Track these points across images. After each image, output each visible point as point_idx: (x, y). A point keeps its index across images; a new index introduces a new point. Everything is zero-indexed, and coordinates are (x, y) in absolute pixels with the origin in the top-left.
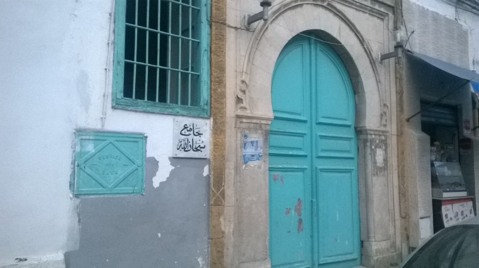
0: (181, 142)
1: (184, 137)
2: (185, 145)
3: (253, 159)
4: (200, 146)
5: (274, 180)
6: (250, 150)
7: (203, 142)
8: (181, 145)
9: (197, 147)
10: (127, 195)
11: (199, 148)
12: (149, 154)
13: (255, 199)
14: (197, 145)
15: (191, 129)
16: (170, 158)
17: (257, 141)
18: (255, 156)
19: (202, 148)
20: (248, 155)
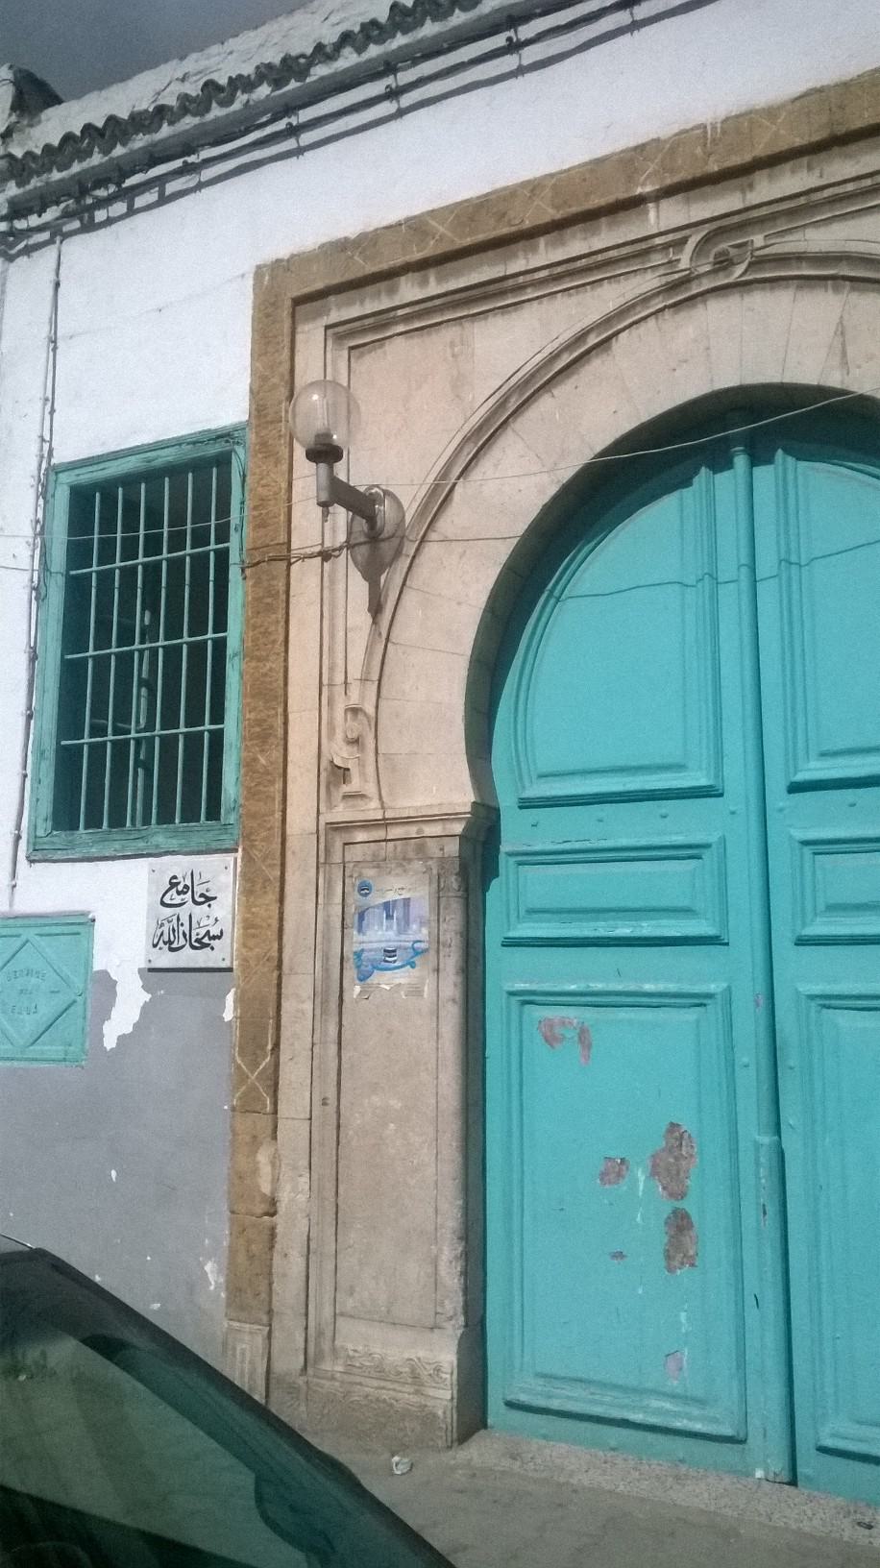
0: (162, 925)
1: (169, 911)
2: (172, 936)
3: (393, 965)
4: (208, 932)
5: (546, 1040)
6: (380, 933)
7: (216, 920)
8: (162, 934)
9: (200, 937)
10: (53, 1065)
11: (206, 940)
12: (97, 967)
13: (396, 1104)
14: (203, 932)
15: (186, 886)
16: (140, 971)
17: (407, 902)
18: (397, 953)
19: (214, 938)
20: (371, 950)
